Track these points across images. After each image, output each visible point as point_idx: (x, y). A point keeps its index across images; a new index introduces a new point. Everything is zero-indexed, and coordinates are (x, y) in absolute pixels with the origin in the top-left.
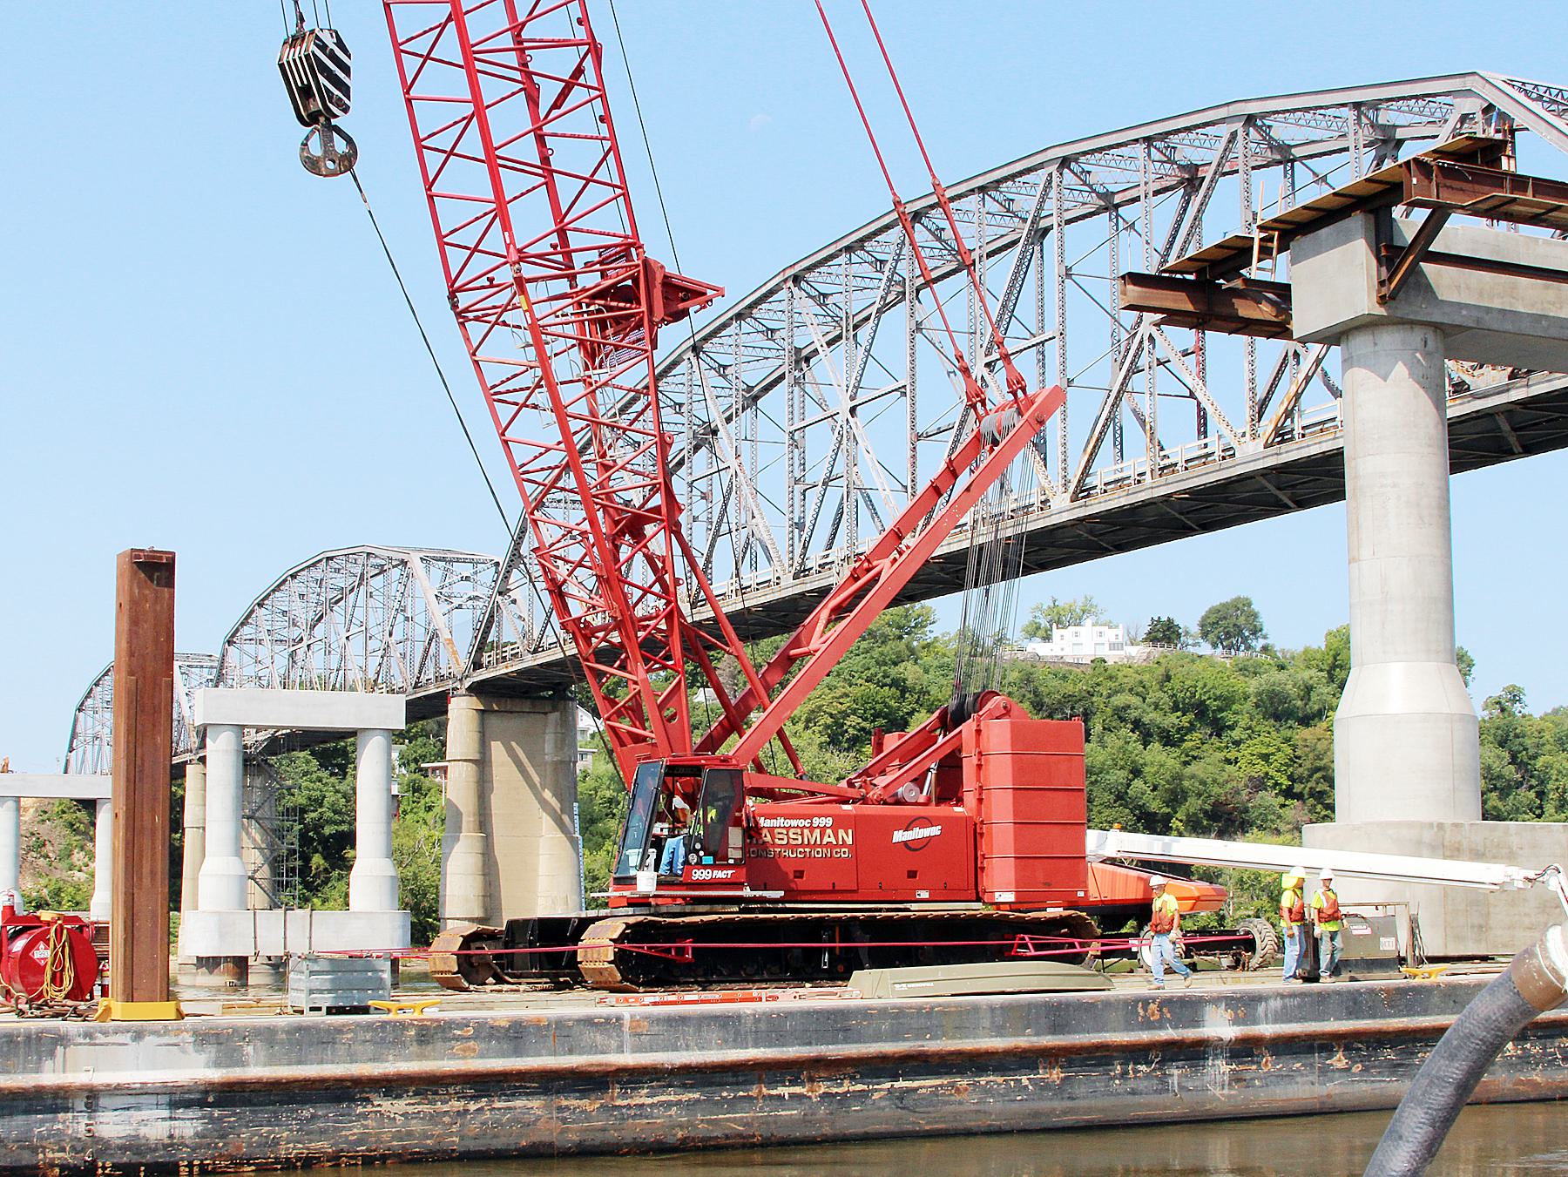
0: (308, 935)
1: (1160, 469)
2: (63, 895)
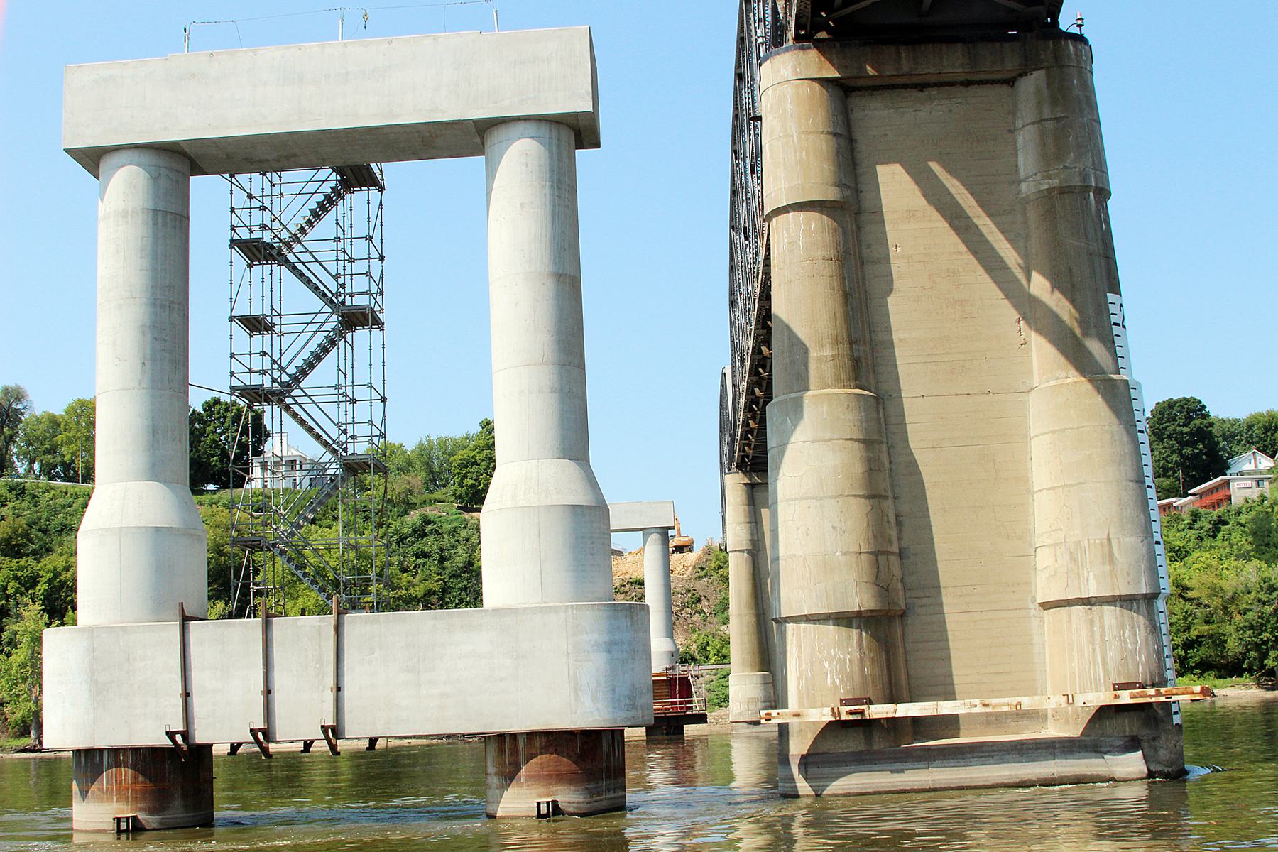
0: (331, 682)
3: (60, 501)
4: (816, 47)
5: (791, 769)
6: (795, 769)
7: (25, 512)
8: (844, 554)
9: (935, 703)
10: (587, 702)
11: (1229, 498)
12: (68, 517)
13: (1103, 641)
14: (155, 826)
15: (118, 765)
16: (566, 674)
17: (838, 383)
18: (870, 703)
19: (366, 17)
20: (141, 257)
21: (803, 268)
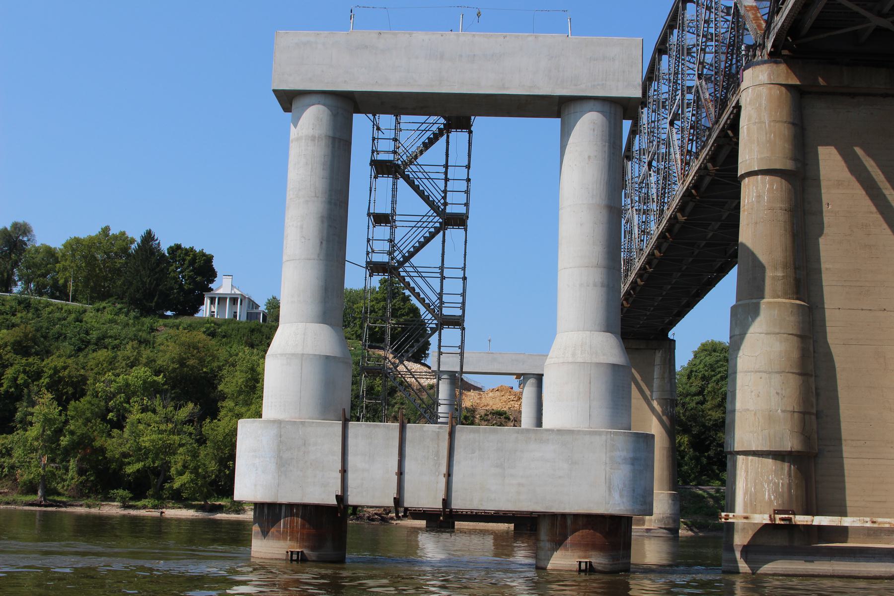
0: (444, 469)
3: (57, 315)
5: (735, 554)
6: (738, 555)
7: (31, 322)
8: (783, 411)
9: (840, 518)
10: (616, 496)
12: (64, 328)
14: (314, 558)
15: (292, 515)
16: (604, 477)
17: (785, 295)
18: (794, 514)
19: (479, 15)
20: (323, 169)
21: (766, 215)
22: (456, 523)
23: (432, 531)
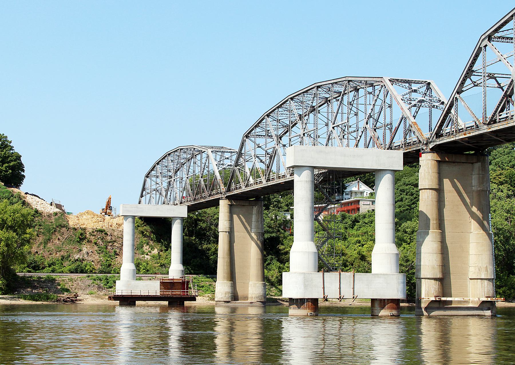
0: (352, 287)
1: (459, 130)
2: (140, 266)
4: (436, 153)
11: (358, 209)
13: (484, 288)
22: (136, 302)
23: (172, 307)
